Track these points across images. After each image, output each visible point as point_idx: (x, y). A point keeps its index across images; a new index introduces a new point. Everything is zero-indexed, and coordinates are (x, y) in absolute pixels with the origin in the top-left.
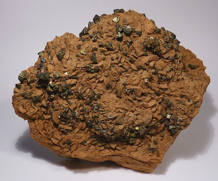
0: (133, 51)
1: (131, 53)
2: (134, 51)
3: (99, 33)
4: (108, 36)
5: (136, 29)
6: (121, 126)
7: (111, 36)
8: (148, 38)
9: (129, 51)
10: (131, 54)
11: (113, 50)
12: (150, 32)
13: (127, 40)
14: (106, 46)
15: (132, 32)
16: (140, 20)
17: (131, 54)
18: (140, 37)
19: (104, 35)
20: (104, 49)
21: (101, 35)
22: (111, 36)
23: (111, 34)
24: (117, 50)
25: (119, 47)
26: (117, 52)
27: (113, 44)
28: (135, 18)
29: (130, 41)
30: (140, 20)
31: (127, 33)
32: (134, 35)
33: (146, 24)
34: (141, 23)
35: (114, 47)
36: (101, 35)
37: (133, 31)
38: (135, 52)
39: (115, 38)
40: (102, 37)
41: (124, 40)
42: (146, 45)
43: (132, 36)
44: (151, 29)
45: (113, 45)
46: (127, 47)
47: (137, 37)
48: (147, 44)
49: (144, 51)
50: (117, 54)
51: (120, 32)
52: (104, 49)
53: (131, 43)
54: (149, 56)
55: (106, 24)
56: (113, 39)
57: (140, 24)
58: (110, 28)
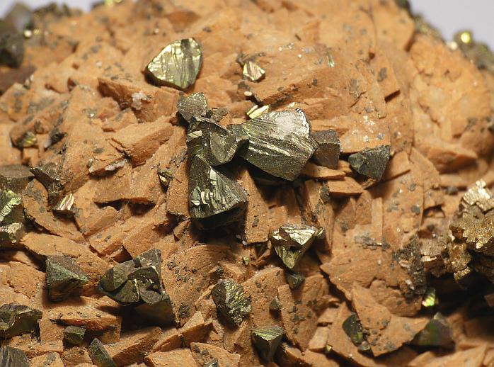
0: (329, 315)
1: (310, 335)
2: (335, 316)
3: (36, 185)
4: (117, 204)
5: (341, 132)
6: (120, 141)
7: (140, 207)
8: (451, 204)
9: (297, 320)
10: (319, 340)
11: (168, 323)
12: (461, 149)
13: (282, 232)
14: (113, 293)
15: (314, 160)
16: (372, 56)
17: (319, 340)
18: (375, 196)
19: (81, 199)
20: (90, 310)
21: (53, 201)
22: (140, 207)
23: (138, 184)
24: (197, 320)
25: (218, 295)
26: (203, 333)
27: (171, 267)
28: (330, 36)
29: (303, 235)
30: (372, 56)
31: (275, 170)
32: (335, 187)
33: (420, 84)
34: (382, 76)
35: (174, 292)
36: (53, 201)
37: (328, 153)
38: (352, 326)
39: (173, 220)
40: (67, 217)
41: (253, 235)
42: (438, 263)
43: (314, 199)
44: (471, 122)
45: (166, 276)
46: (284, 288)
47: (357, 196)
48: (446, 254)
49: (424, 312)
50: (201, 346)
51: (218, 168)
52: (90, 310)
53: (317, 249)
54: (465, 348)
55: (90, 97)
56: (163, 230)
57: (377, 92)
58: (132, 133)
